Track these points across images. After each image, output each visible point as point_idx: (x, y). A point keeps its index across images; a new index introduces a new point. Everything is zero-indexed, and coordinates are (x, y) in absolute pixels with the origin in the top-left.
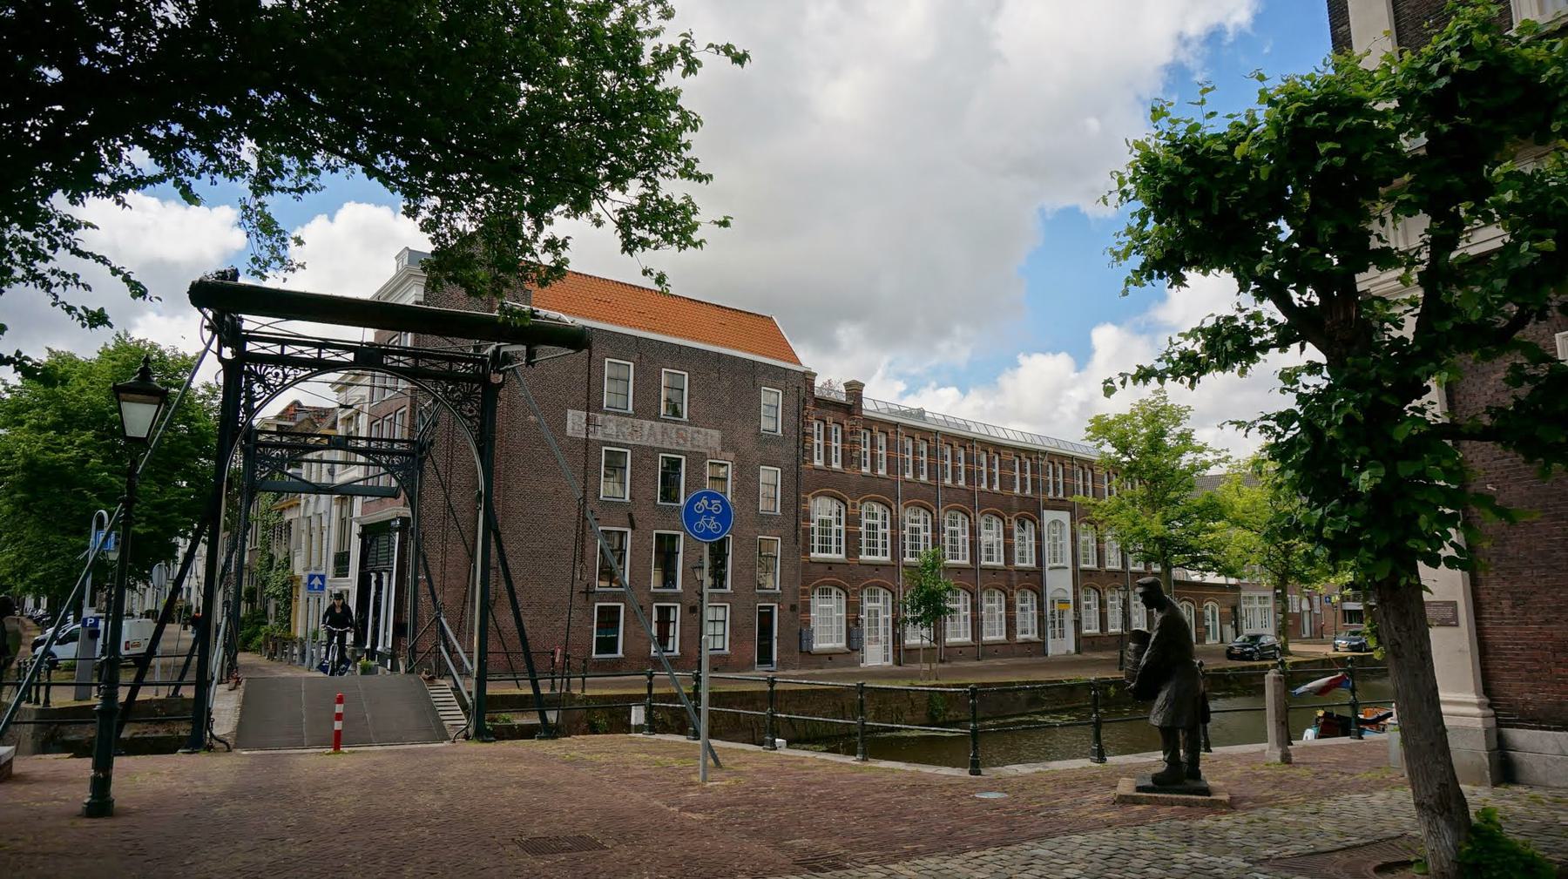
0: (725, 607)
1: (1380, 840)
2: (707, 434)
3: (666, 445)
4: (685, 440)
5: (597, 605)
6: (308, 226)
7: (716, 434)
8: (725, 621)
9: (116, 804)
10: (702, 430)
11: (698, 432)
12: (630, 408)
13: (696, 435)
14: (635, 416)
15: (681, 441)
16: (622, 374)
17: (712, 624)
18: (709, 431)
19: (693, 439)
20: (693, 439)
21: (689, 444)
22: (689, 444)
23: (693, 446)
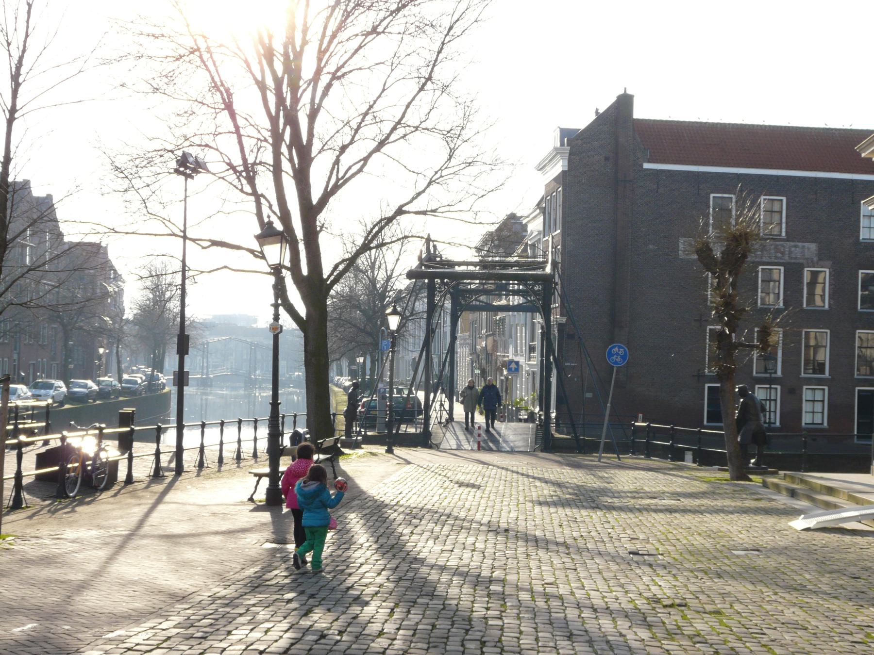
0: (824, 390)
1: (720, 576)
2: (803, 247)
3: (765, 260)
4: (783, 254)
5: (707, 386)
6: (236, 112)
7: (813, 247)
8: (823, 401)
9: (117, 443)
10: (800, 244)
11: (796, 246)
12: (784, 234)
13: (793, 249)
14: (787, 240)
15: (779, 255)
16: (776, 207)
17: (811, 403)
18: (806, 245)
19: (790, 252)
20: (790, 252)
21: (787, 257)
22: (787, 257)
23: (790, 258)
